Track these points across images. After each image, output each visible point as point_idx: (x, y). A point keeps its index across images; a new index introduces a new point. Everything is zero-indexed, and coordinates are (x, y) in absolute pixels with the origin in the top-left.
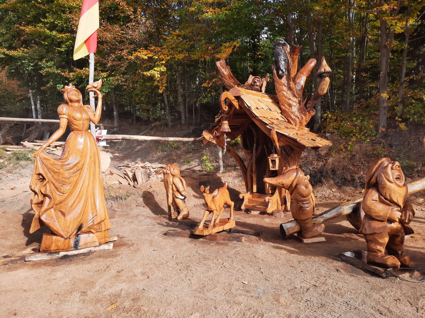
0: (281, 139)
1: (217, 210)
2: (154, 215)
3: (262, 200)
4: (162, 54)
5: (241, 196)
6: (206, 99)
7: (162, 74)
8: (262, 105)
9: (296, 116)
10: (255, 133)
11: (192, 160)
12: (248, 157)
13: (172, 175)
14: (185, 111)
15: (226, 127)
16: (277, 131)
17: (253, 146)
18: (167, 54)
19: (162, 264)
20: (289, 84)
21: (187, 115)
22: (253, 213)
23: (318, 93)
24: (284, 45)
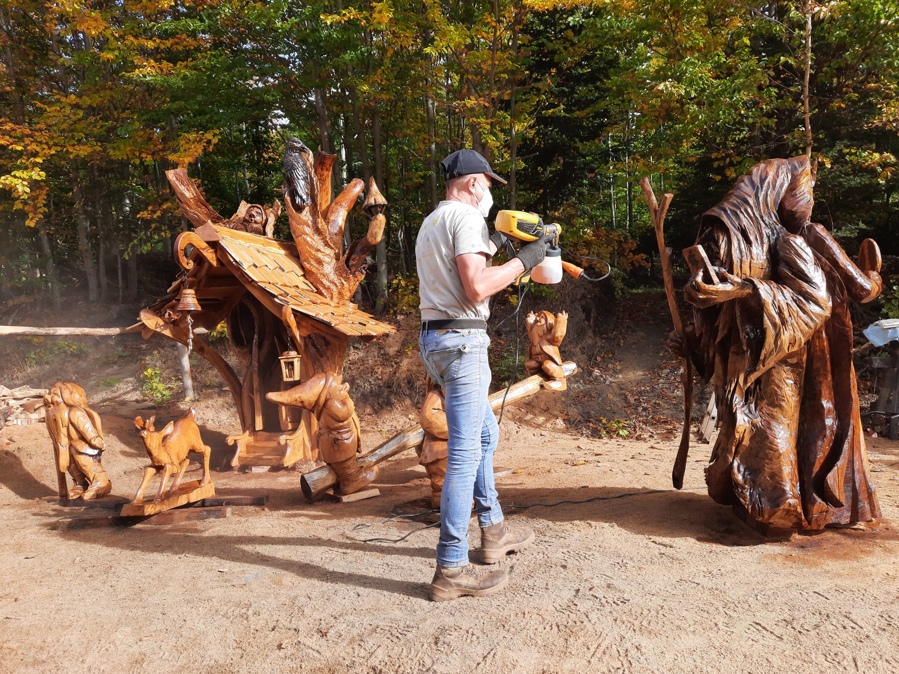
0: (304, 323)
1: (172, 463)
2: (22, 501)
3: (273, 444)
4: (36, 141)
5: (230, 441)
6: (149, 244)
7: (34, 185)
8: (265, 260)
9: (331, 282)
10: (255, 315)
11: (119, 381)
12: (244, 361)
13: (68, 405)
14: (98, 270)
15: (190, 300)
16: (295, 307)
17: (253, 338)
18: (47, 144)
19: (49, 575)
20: (315, 223)
21: (104, 280)
22: (255, 470)
23: (367, 240)
24: (302, 150)
